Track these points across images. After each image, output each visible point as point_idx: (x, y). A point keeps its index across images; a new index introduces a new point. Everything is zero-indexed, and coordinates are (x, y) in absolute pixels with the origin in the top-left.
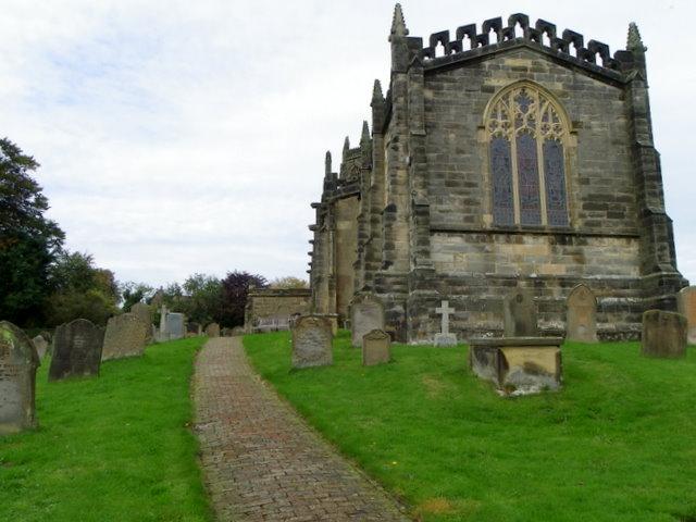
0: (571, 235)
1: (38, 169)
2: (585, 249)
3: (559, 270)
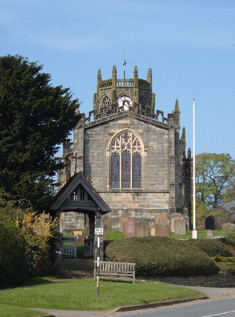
0: (141, 192)
1: (43, 67)
2: (147, 197)
3: (137, 206)
